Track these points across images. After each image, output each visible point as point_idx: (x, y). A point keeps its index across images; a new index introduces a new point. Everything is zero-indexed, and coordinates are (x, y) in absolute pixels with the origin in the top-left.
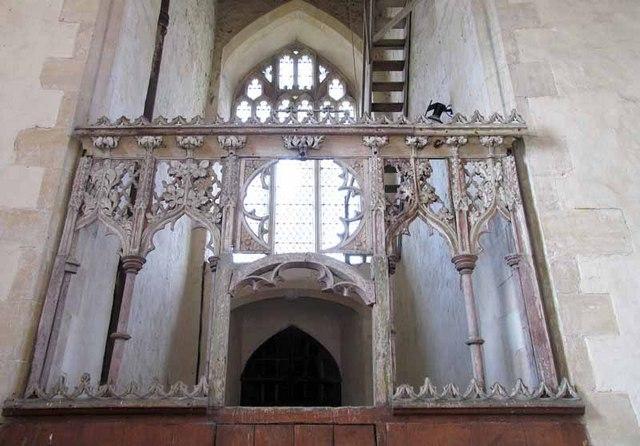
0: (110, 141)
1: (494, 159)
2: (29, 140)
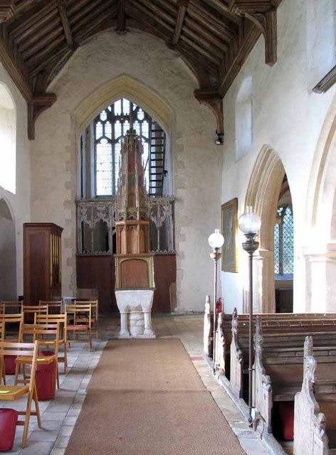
2: (66, 203)
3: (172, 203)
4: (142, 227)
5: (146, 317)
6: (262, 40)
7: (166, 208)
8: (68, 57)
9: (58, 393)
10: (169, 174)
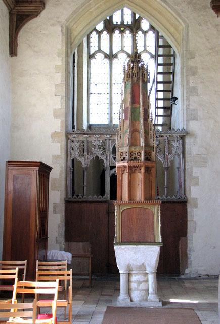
0: (76, 136)
1: (177, 140)
3: (183, 138)
4: (148, 170)
5: (151, 278)
7: (175, 144)
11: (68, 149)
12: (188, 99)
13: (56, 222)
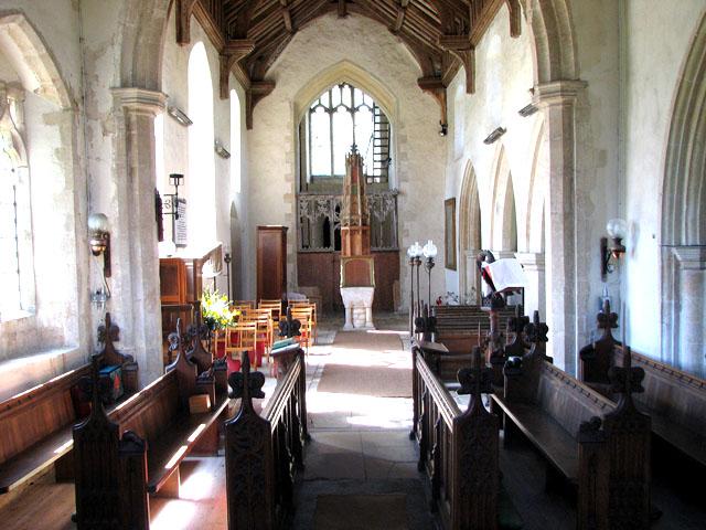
3: (395, 197)
4: (364, 232)
5: (369, 312)
6: (462, 72)
7: (389, 202)
8: (288, 42)
9: (180, 496)
10: (392, 161)
11: (298, 208)
12: (399, 164)
13: (291, 268)
